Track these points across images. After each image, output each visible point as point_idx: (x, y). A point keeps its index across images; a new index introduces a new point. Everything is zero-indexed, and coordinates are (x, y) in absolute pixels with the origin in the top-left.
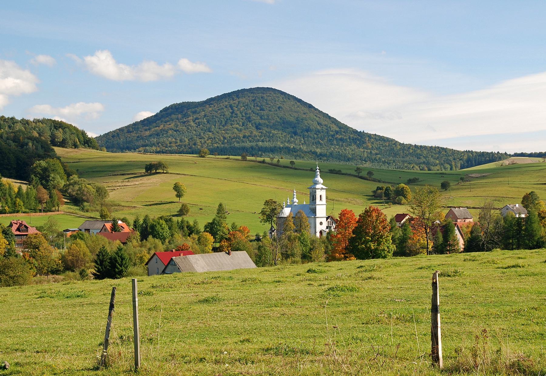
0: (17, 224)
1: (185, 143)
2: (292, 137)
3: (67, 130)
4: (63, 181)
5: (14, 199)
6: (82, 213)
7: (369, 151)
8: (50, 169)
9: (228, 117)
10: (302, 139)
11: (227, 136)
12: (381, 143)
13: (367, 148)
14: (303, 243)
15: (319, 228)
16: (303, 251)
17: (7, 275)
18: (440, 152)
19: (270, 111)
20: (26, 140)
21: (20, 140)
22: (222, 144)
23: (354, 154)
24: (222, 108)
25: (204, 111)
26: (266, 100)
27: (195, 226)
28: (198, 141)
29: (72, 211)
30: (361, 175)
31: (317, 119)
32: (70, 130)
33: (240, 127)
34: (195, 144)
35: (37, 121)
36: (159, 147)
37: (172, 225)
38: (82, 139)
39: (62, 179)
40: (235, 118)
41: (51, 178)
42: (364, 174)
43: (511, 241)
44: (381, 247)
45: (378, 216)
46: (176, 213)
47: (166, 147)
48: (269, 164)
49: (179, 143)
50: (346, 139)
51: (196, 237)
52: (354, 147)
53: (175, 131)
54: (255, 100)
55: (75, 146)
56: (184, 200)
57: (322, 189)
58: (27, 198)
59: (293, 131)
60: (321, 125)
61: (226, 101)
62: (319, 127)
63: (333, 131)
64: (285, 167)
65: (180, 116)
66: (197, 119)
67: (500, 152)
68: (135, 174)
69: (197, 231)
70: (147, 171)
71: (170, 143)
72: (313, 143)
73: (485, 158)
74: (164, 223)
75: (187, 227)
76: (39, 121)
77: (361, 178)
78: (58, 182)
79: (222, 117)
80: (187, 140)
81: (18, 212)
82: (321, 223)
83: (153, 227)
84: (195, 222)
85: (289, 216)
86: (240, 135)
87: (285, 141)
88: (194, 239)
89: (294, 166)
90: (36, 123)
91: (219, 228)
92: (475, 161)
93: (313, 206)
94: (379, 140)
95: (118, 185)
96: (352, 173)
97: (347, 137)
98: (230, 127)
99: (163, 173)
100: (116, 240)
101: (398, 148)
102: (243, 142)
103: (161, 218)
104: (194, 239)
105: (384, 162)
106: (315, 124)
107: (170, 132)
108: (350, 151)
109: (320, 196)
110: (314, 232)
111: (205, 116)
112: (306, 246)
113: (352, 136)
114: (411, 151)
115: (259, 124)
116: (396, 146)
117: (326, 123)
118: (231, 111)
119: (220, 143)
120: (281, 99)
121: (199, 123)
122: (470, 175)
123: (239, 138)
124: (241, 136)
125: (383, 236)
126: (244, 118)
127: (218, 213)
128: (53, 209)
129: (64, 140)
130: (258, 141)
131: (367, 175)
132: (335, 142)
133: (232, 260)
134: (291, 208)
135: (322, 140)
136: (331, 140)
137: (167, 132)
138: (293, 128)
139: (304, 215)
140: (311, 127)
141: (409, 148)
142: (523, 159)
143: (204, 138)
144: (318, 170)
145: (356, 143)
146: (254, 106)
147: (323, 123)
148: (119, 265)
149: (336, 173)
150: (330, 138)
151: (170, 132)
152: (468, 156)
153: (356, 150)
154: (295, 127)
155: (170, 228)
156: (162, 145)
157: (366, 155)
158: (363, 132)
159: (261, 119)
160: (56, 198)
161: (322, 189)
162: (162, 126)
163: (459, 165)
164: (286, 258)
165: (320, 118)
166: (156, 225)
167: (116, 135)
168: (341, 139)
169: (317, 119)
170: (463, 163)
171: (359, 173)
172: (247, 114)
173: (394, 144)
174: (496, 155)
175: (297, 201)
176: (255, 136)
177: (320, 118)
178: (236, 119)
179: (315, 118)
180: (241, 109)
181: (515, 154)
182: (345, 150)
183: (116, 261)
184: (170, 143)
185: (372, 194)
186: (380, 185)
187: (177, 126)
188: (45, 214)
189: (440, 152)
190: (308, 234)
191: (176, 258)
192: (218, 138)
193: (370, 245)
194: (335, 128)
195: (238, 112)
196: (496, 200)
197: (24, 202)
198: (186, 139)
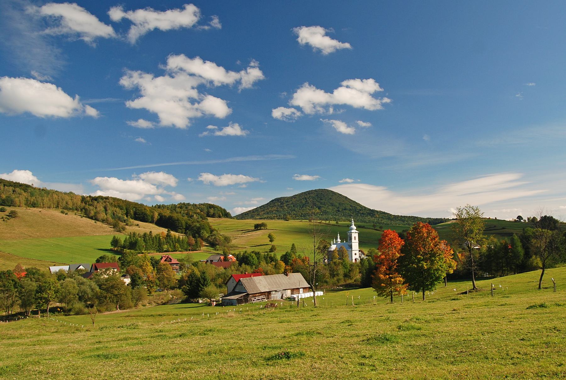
0: (165, 257)
2: (337, 213)
3: (216, 209)
4: (208, 234)
5: (175, 244)
6: (214, 251)
8: (201, 228)
9: (304, 203)
13: (376, 217)
14: (344, 267)
15: (354, 257)
16: (345, 272)
17: (112, 293)
19: (326, 200)
20: (193, 214)
21: (190, 214)
24: (301, 200)
25: (291, 201)
27: (274, 257)
29: (209, 250)
30: (376, 228)
31: (350, 204)
32: (218, 209)
35: (200, 205)
37: (259, 256)
38: (224, 213)
39: (207, 233)
41: (201, 233)
43: (501, 261)
44: (436, 267)
50: (365, 214)
51: (274, 263)
52: (369, 217)
53: (277, 211)
55: (220, 217)
56: (274, 243)
57: (356, 232)
58: (182, 243)
65: (279, 204)
66: (288, 205)
68: (249, 230)
69: (276, 260)
70: (255, 228)
71: (274, 217)
74: (254, 255)
75: (269, 258)
76: (202, 204)
78: (205, 235)
81: (176, 251)
82: (355, 254)
83: (247, 258)
85: (335, 250)
88: (273, 265)
89: (338, 225)
90: (200, 206)
93: (350, 244)
98: (305, 208)
99: (264, 229)
100: (220, 266)
103: (253, 252)
104: (273, 265)
107: (274, 212)
110: (351, 260)
111: (292, 203)
112: (346, 268)
115: (320, 207)
117: (355, 206)
120: (331, 194)
125: (436, 254)
127: (292, 250)
128: (197, 249)
129: (214, 214)
132: (359, 215)
133: (289, 280)
134: (336, 245)
137: (273, 212)
138: (337, 208)
139: (345, 249)
141: (398, 217)
143: (291, 214)
144: (353, 221)
147: (353, 205)
148: (202, 285)
150: (357, 213)
151: (274, 212)
152: (429, 221)
154: (339, 208)
155: (258, 259)
159: (321, 204)
160: (199, 243)
161: (356, 232)
162: (270, 209)
164: (333, 277)
166: (249, 257)
168: (363, 213)
169: (350, 204)
175: (340, 241)
182: (365, 218)
183: (200, 282)
187: (278, 209)
188: (192, 252)
190: (347, 260)
191: (243, 280)
193: (423, 265)
194: (359, 208)
197: (180, 245)
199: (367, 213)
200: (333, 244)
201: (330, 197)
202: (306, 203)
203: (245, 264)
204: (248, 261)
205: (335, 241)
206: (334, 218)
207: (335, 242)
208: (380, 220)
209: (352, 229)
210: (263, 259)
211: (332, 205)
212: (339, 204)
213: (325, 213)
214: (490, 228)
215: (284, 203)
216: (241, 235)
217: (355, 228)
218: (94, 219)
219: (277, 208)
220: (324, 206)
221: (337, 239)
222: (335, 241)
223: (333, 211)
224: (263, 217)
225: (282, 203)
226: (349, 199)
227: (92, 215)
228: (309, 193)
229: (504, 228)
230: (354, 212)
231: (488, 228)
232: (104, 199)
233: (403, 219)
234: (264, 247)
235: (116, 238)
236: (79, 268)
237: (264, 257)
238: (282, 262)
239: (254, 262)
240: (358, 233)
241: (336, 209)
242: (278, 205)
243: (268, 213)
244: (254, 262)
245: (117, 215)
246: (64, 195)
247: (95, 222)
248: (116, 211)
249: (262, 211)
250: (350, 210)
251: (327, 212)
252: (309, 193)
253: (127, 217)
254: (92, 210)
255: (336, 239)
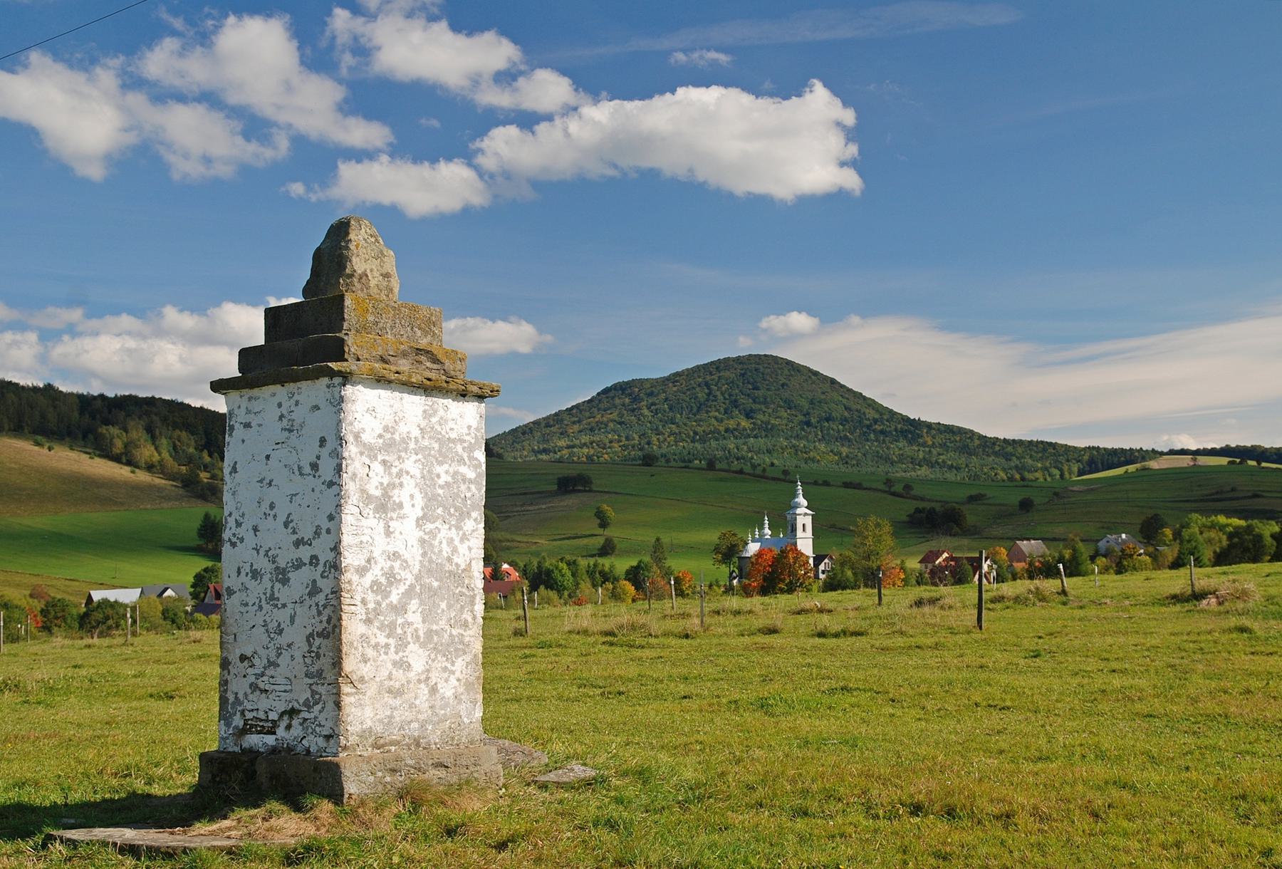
1: (633, 442)
2: (803, 429)
7: (927, 449)
9: (702, 400)
10: (820, 433)
11: (699, 429)
12: (948, 437)
13: (924, 445)
18: (1044, 450)
19: (768, 390)
22: (692, 442)
23: (902, 455)
25: (664, 392)
26: (763, 374)
27: (611, 571)
28: (654, 439)
30: (892, 490)
31: (844, 401)
33: (721, 416)
34: (649, 443)
36: (593, 448)
37: (577, 570)
40: (713, 401)
42: (898, 488)
45: (796, 559)
46: (596, 552)
47: (604, 448)
48: (749, 474)
49: (624, 442)
50: (890, 432)
51: (611, 586)
53: (620, 423)
54: (745, 374)
57: (806, 514)
59: (804, 420)
60: (851, 410)
61: (699, 377)
62: (846, 414)
63: (869, 419)
64: (774, 479)
67: (1144, 449)
70: (559, 488)
71: (611, 442)
72: (837, 439)
73: (1119, 458)
74: (565, 566)
75: (600, 573)
77: (894, 494)
79: (693, 400)
80: (636, 437)
84: (612, 566)
86: (721, 428)
87: (791, 436)
88: (607, 589)
91: (647, 574)
92: (1102, 464)
93: (793, 541)
94: (945, 432)
95: (515, 510)
96: (880, 488)
97: (893, 427)
99: (585, 491)
101: (976, 444)
102: (725, 438)
104: (607, 589)
105: (951, 467)
106: (841, 408)
107: (611, 425)
108: (896, 450)
109: (804, 525)
111: (666, 399)
113: (899, 426)
114: (997, 448)
115: (752, 411)
116: (972, 440)
117: (859, 407)
118: (707, 391)
119: (689, 441)
120: (786, 372)
121: (656, 410)
122: (1071, 488)
123: (719, 433)
124: (722, 429)
126: (727, 401)
130: (749, 436)
131: (903, 490)
132: (872, 436)
135: (852, 434)
136: (866, 432)
137: (606, 425)
138: (804, 415)
140: (833, 414)
141: (994, 444)
142: (1177, 459)
143: (664, 434)
144: (799, 487)
145: (906, 437)
146: (743, 384)
147: (854, 407)
149: (854, 488)
150: (865, 430)
151: (611, 425)
153: (907, 449)
155: (573, 575)
156: (597, 445)
157: (921, 456)
158: (919, 419)
159: (754, 402)
161: (806, 514)
162: (599, 416)
163: (1075, 469)
165: (848, 399)
166: (553, 570)
167: (528, 431)
168: (882, 432)
169: (844, 401)
170: (1081, 467)
171: (890, 487)
172: (732, 395)
173: (970, 438)
174: (1137, 454)
175: (770, 533)
176: (745, 429)
177: (848, 399)
178: (714, 403)
179: (841, 399)
180: (723, 389)
181: (1170, 450)
184: (611, 442)
185: (906, 519)
186: (921, 505)
189: (1044, 450)
192: (686, 432)
194: (871, 414)
195: (718, 393)
196: (1103, 528)
198: (635, 435)
199: (896, 430)
200: (752, 542)
201: (783, 381)
202: (708, 400)
203: (547, 588)
204: (552, 582)
205: (757, 533)
206: (794, 446)
207: (757, 536)
208: (934, 452)
209: (797, 506)
210: (585, 576)
211: (789, 405)
212: (812, 403)
213: (766, 430)
214: (1217, 493)
215: (642, 400)
216: (522, 506)
217: (805, 503)
218: (124, 461)
219: (620, 415)
220: (763, 406)
221: (764, 528)
222: (757, 533)
223: (791, 425)
224: (577, 442)
225: (636, 399)
226: (842, 386)
227: (118, 452)
228: (717, 368)
229: (1256, 496)
230: (855, 428)
231: (1213, 494)
232: (145, 406)
233: (1010, 449)
234: (585, 541)
235: (213, 518)
236: (166, 594)
237: (588, 572)
238: (627, 582)
239: (565, 583)
240: (812, 515)
241: (801, 418)
242: (624, 405)
243: (592, 430)
244: (565, 583)
245: (184, 451)
246: (32, 393)
247: (133, 472)
248: (179, 441)
249: (574, 423)
250: (844, 421)
251: (773, 426)
252: (717, 368)
253: (210, 455)
254: (118, 437)
255: (761, 528)
